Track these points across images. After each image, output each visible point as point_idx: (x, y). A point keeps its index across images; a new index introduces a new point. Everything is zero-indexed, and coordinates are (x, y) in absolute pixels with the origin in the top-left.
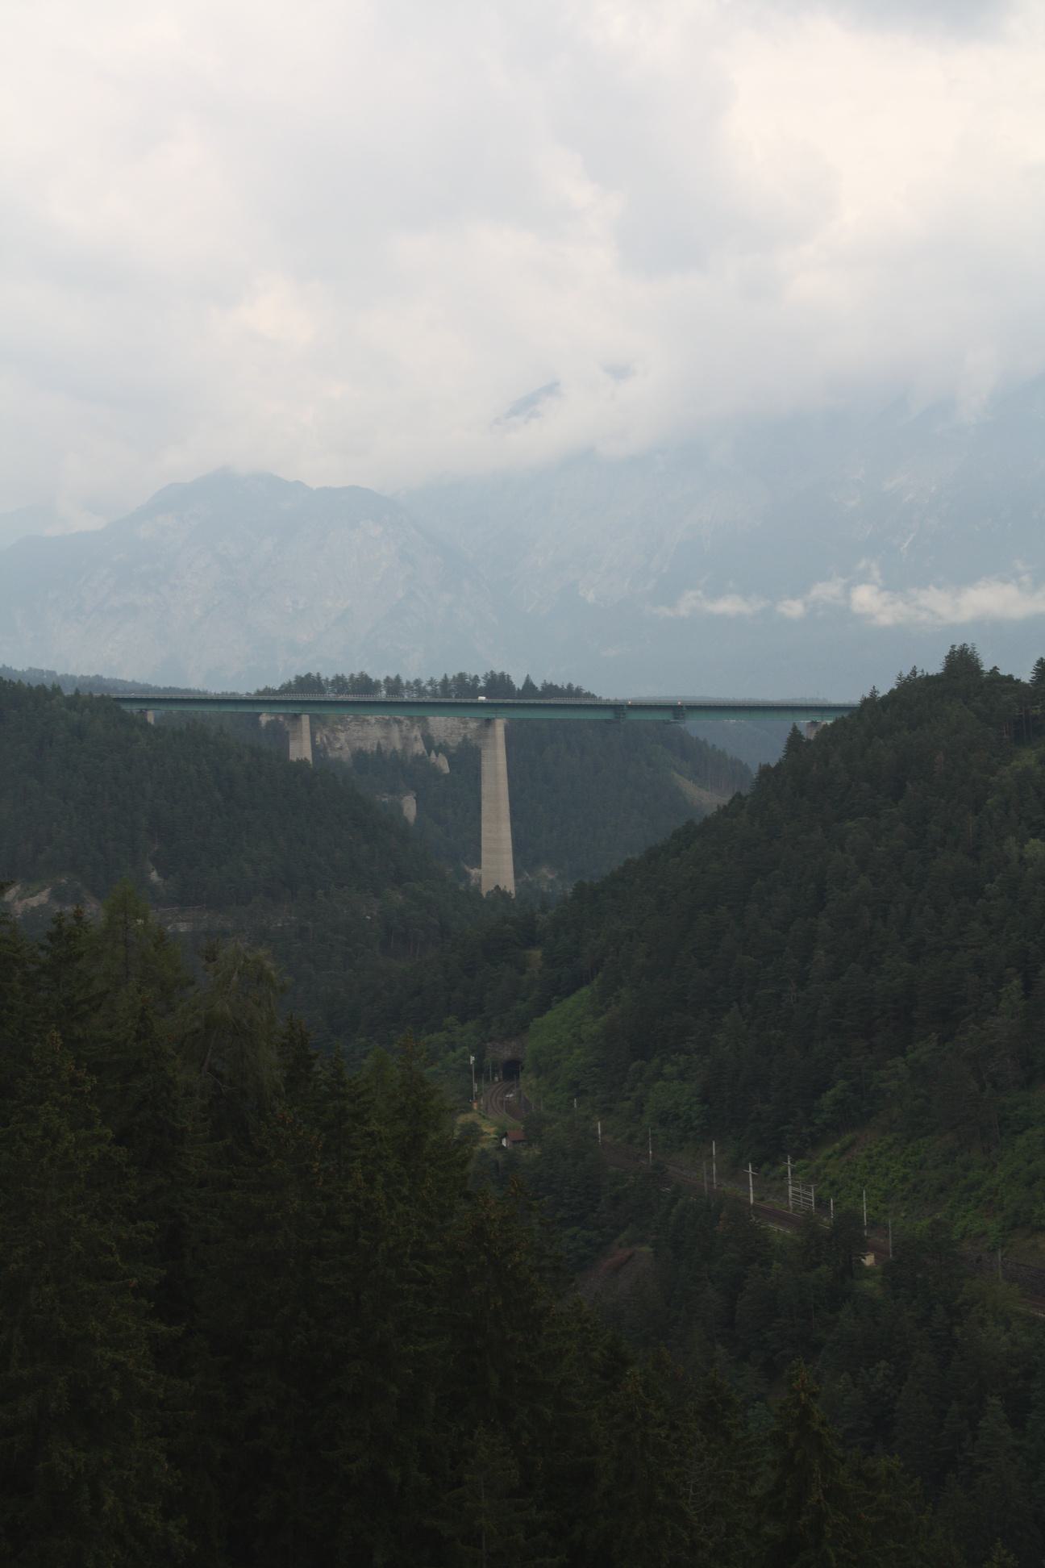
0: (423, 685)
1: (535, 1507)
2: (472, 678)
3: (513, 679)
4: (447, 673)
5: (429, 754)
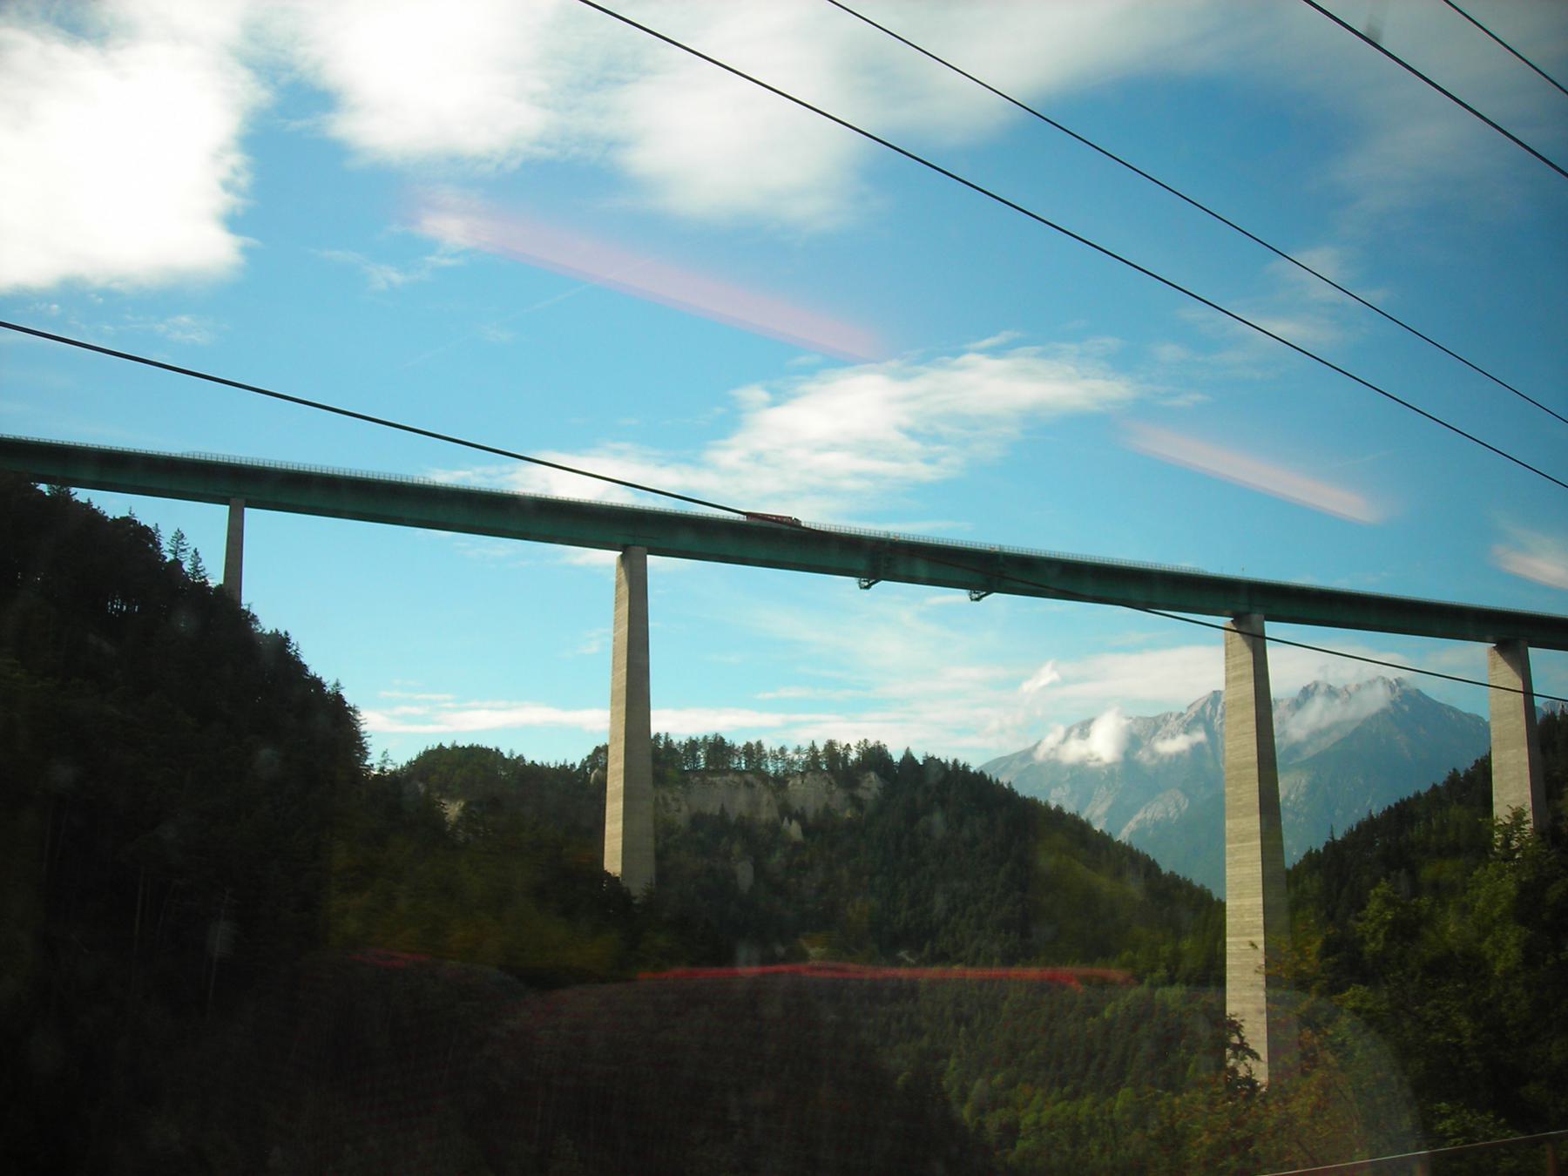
0: (788, 753)
1: (1383, 879)
2: (844, 746)
3: (890, 750)
4: (959, 758)
5: (783, 820)
